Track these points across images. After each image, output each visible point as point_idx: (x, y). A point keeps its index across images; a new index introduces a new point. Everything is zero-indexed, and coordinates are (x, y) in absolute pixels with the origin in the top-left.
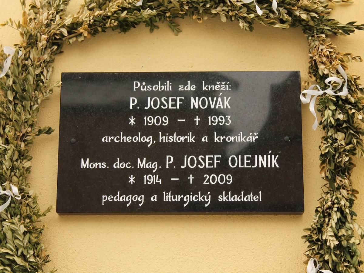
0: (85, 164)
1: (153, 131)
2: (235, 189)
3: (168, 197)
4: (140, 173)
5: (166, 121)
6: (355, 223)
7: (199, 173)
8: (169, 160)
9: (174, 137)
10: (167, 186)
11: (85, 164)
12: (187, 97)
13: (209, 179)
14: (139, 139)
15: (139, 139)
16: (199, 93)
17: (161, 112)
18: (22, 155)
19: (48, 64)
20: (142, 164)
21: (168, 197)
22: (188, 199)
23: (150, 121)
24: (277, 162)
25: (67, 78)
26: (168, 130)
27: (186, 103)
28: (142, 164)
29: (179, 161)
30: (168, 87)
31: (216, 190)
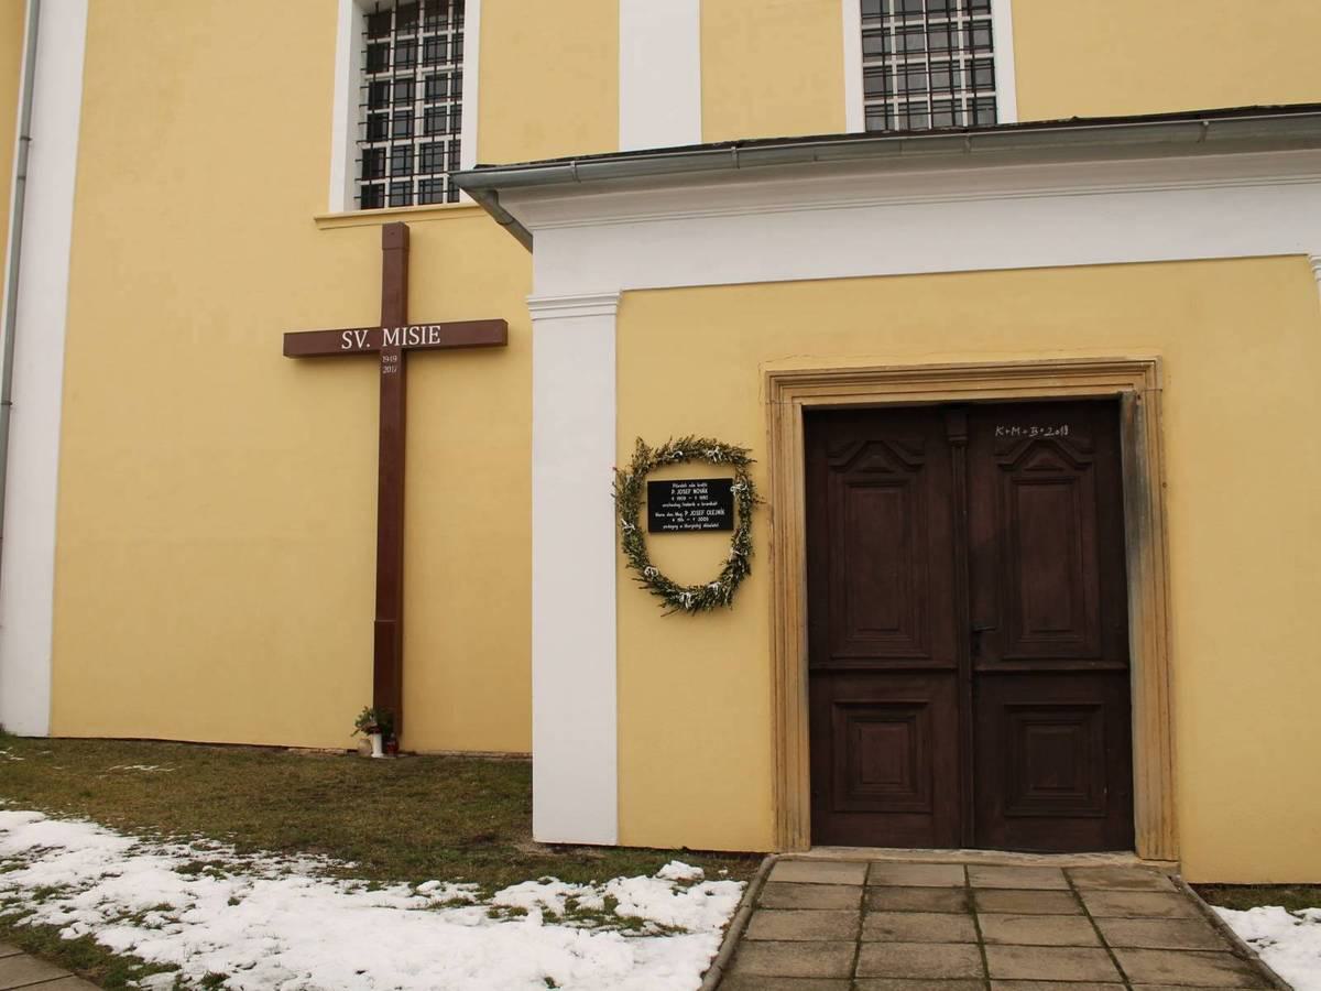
0: (657, 515)
1: (680, 502)
2: (709, 523)
3: (686, 526)
4: (677, 518)
5: (685, 498)
6: (759, 505)
7: (697, 517)
8: (686, 513)
9: (962, 52)
10: (686, 522)
11: (657, 515)
12: (692, 488)
13: (700, 519)
14: (675, 505)
15: (675, 505)
16: (696, 488)
17: (683, 495)
18: (635, 513)
19: (642, 478)
20: (677, 514)
21: (686, 526)
22: (693, 526)
23: (679, 498)
24: (575, 875)
25: (649, 483)
26: (685, 502)
27: (692, 492)
28: (677, 514)
29: (690, 513)
30: (685, 486)
31: (703, 523)
